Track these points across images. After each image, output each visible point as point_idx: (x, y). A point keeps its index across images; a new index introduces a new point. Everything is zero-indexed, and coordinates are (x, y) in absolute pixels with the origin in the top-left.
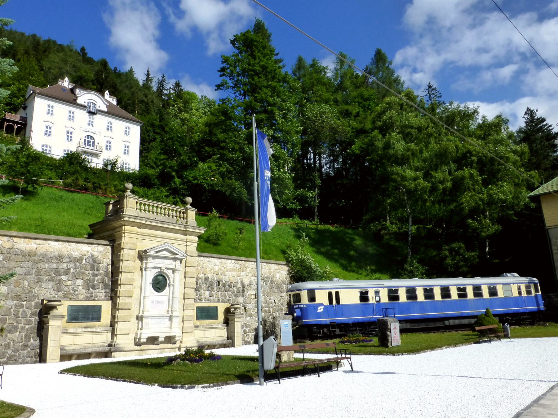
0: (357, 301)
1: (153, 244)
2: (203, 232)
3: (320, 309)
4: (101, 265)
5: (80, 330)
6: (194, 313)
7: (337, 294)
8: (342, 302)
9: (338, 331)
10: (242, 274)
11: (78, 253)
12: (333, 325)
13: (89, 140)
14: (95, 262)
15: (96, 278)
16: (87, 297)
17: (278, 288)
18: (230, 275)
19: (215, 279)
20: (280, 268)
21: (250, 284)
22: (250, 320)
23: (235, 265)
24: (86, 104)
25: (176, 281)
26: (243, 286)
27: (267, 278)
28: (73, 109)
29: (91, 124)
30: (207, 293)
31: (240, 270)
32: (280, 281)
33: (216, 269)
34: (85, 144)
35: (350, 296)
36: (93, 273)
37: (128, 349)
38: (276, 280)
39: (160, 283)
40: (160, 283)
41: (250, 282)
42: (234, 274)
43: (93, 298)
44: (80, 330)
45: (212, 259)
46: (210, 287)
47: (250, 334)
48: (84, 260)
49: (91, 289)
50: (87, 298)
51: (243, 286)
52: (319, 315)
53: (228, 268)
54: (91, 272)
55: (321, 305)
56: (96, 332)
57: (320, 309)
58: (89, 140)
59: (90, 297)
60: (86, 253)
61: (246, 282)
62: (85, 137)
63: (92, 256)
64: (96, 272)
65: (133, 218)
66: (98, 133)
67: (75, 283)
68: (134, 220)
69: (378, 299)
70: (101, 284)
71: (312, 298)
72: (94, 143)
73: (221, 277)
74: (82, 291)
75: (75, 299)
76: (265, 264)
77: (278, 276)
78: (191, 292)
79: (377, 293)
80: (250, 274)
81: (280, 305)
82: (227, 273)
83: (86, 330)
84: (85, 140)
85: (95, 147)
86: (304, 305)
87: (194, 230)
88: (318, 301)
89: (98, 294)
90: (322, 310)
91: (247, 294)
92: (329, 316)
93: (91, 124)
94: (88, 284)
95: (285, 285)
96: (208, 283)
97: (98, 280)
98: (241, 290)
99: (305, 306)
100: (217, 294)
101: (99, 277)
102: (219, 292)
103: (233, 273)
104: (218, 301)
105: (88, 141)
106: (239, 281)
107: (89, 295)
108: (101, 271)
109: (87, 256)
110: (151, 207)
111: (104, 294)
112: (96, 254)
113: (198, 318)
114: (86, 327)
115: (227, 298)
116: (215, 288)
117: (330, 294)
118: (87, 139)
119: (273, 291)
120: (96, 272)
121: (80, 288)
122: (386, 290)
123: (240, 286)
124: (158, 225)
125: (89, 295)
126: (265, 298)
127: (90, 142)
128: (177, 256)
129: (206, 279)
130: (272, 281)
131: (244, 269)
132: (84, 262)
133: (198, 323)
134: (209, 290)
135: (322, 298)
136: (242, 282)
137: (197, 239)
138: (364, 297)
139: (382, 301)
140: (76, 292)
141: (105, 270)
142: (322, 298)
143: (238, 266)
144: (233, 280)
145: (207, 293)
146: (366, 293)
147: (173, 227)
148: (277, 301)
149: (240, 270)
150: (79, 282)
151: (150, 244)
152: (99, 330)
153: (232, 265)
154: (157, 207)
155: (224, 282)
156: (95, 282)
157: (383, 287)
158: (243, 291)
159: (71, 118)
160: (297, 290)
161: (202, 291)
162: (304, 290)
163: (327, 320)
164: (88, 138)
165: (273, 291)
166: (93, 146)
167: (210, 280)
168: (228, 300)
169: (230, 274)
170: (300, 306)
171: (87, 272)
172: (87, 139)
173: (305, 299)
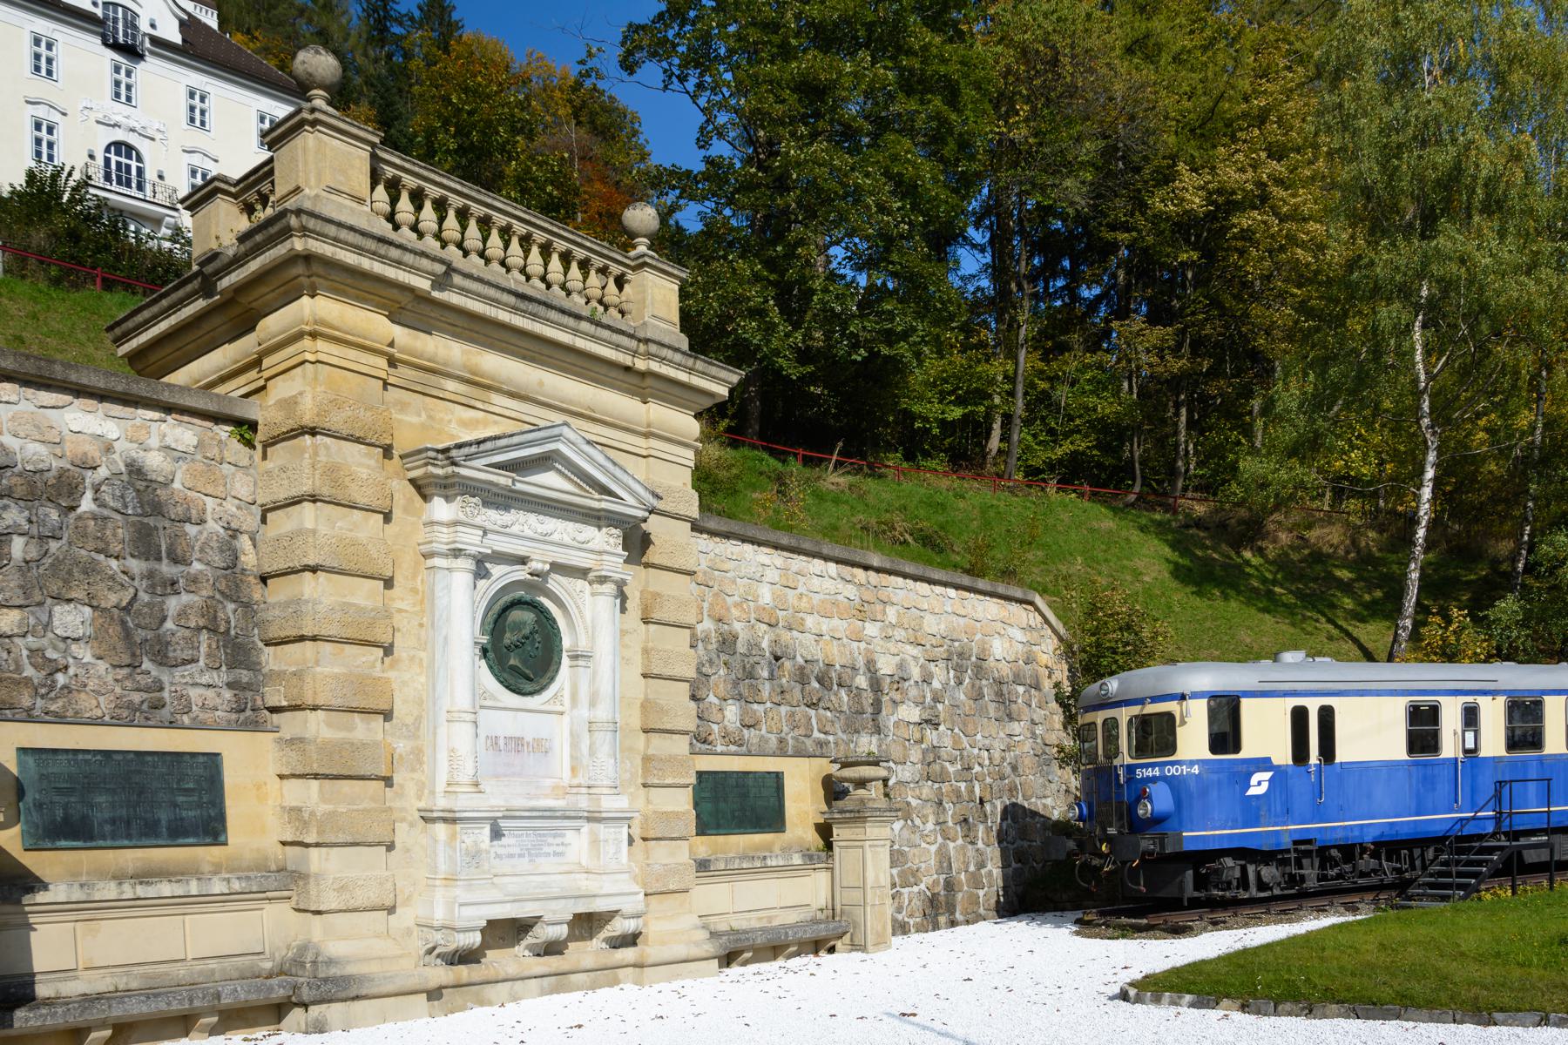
0: (1396, 749)
1: (486, 424)
2: (723, 391)
3: (1259, 784)
4: (191, 530)
5: (109, 891)
6: (682, 802)
7: (1327, 715)
8: (1343, 754)
9: (1310, 872)
10: (871, 629)
11: (42, 450)
12: (1304, 848)
13: (123, 160)
14: (157, 509)
15: (173, 604)
16: (130, 706)
17: (1002, 699)
18: (824, 628)
19: (765, 644)
20: (1003, 614)
21: (900, 680)
22: (906, 833)
23: (841, 585)
24: (99, 12)
25: (588, 620)
26: (876, 685)
27: (960, 655)
28: (44, 26)
29: (123, 93)
30: (732, 712)
31: (862, 612)
32: (1006, 670)
33: (766, 595)
34: (108, 177)
35: (1371, 731)
36: (150, 575)
37: (390, 988)
38: (991, 663)
39: (522, 648)
40: (522, 648)
41: (901, 666)
42: (839, 625)
43: (165, 713)
44: (109, 891)
45: (748, 547)
46: (744, 683)
47: (905, 891)
48: (89, 495)
49: (147, 665)
50: (126, 716)
51: (876, 685)
52: (1253, 810)
53: (816, 599)
54: (136, 566)
55: (1264, 764)
56: (205, 899)
57: (1259, 784)
58: (123, 160)
59: (151, 711)
60: (93, 451)
61: (886, 666)
62: (108, 150)
63: (136, 471)
64: (166, 569)
65: (359, 250)
66: (158, 136)
67: (47, 626)
68: (366, 264)
69: (1470, 745)
70: (204, 636)
71: (1225, 736)
72: (140, 171)
73: (786, 636)
74: (94, 670)
75: (60, 719)
76: (952, 592)
77: (998, 648)
78: (678, 706)
79: (1471, 717)
80: (899, 634)
81: (1008, 770)
82: (810, 621)
83: (141, 891)
84: (107, 161)
85: (148, 188)
86: (1192, 763)
87: (683, 376)
88: (1249, 750)
89: (194, 694)
90: (1265, 786)
91: (889, 718)
92: (1288, 814)
93: (123, 93)
94: (127, 635)
95: (1021, 689)
96: (736, 662)
97: (183, 614)
98: (868, 698)
99: (1196, 770)
100: (774, 718)
101: (185, 598)
102: (784, 709)
103: (836, 622)
104: (782, 752)
105: (119, 164)
106: (861, 663)
107: (137, 697)
108: (197, 566)
109: (103, 472)
110: (451, 221)
111: (228, 694)
112: (154, 461)
113: (702, 829)
114: (145, 876)
115: (816, 734)
116: (766, 689)
117: (1299, 716)
118: (114, 158)
119: (982, 712)
120: (166, 569)
121: (85, 653)
122: (1501, 701)
123: (862, 681)
124: (504, 316)
125: (137, 697)
126: (956, 741)
127: (128, 167)
128: (606, 504)
129: (727, 643)
130: (980, 671)
131: (879, 607)
132: (87, 504)
133: (705, 846)
134: (739, 697)
135: (1266, 732)
136: (871, 666)
137: (689, 426)
138: (1423, 727)
139: (1483, 753)
140: (61, 679)
141: (218, 560)
142: (1266, 732)
143: (850, 591)
144: (837, 655)
145: (732, 712)
146: (1434, 711)
147: (581, 343)
148: (997, 755)
149: (862, 612)
150: (71, 619)
151: (464, 424)
152: (218, 887)
153: (828, 585)
154: (485, 223)
155: (800, 660)
156: (169, 625)
157: (1493, 693)
158: (877, 706)
159: (43, 65)
160: (1155, 699)
161: (712, 698)
162: (1196, 695)
163: (1281, 831)
164: (118, 153)
165: (982, 712)
166: (140, 187)
167: (741, 648)
168: (821, 744)
169: (825, 626)
170: (1172, 771)
171: (114, 563)
172: (114, 158)
173: (1193, 741)
